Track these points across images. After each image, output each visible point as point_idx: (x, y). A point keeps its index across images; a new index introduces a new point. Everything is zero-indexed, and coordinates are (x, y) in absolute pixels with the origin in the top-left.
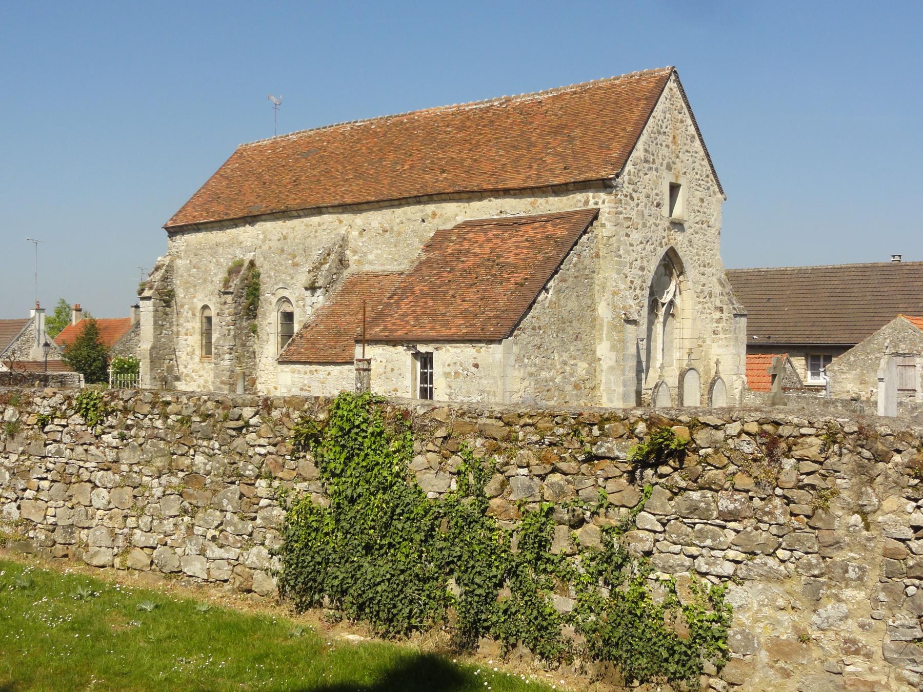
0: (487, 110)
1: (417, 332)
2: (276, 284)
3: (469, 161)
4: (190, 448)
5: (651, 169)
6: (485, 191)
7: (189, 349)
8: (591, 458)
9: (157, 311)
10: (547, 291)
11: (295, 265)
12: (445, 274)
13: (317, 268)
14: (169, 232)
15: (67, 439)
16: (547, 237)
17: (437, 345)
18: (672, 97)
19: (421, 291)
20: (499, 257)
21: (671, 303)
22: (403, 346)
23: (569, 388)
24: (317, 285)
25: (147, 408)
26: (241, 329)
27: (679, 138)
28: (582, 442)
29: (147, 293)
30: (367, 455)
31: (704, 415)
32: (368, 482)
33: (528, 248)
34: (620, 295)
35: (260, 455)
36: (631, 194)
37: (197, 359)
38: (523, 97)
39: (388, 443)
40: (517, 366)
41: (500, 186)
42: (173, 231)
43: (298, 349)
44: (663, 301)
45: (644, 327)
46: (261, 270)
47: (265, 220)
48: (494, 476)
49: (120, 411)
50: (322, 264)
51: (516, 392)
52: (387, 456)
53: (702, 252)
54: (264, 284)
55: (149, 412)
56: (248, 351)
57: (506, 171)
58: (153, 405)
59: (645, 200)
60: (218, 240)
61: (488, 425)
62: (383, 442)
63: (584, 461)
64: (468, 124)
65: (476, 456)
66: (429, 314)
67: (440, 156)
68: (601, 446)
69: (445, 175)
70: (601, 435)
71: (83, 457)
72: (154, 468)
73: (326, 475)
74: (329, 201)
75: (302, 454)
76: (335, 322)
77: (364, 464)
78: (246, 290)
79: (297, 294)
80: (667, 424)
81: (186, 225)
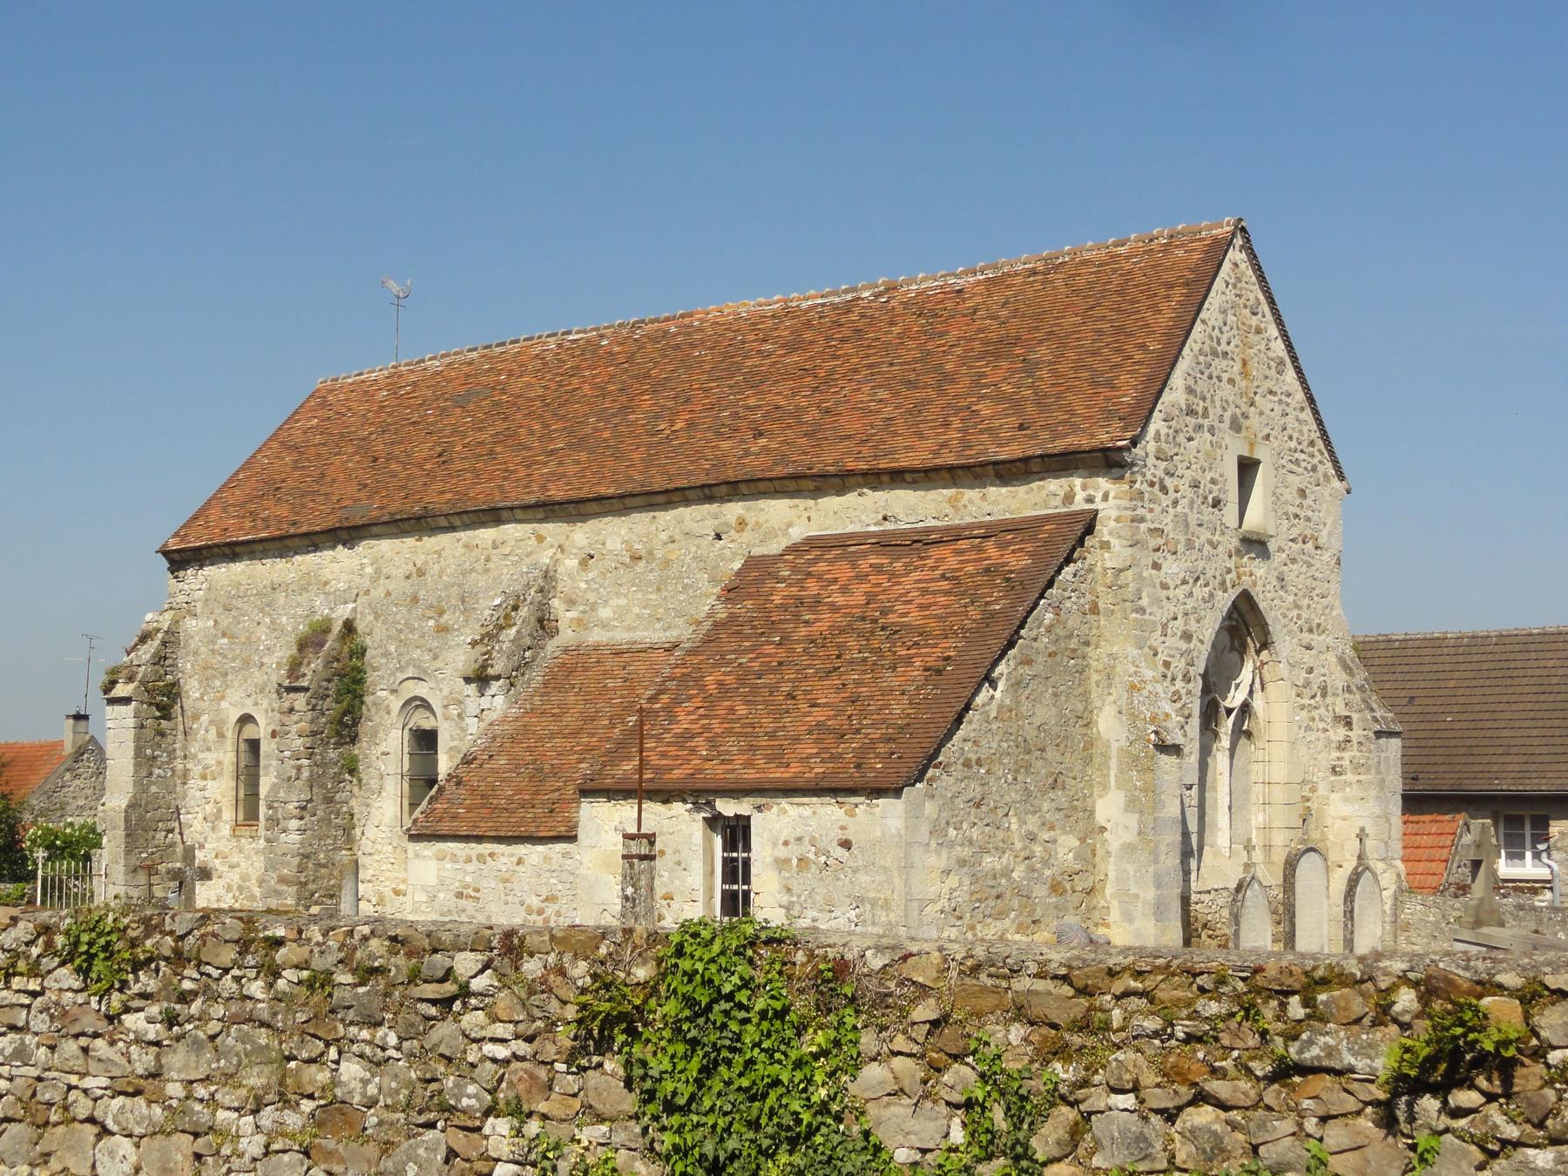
0: (848, 308)
1: (715, 771)
2: (401, 669)
3: (814, 412)
4: (328, 1045)
5: (1199, 427)
6: (852, 473)
7: (209, 808)
8: (1284, 1072)
9: (142, 727)
10: (993, 684)
11: (443, 630)
12: (770, 649)
13: (490, 636)
14: (171, 561)
15: (40, 1023)
16: (987, 570)
17: (760, 801)
18: (1239, 280)
19: (720, 684)
20: (884, 613)
21: (1246, 708)
22: (684, 801)
23: (1040, 891)
24: (490, 671)
25: (229, 954)
26: (324, 765)
27: (1253, 364)
28: (1264, 1034)
29: (121, 690)
30: (750, 1063)
31: (1556, 971)
32: (754, 1125)
33: (946, 593)
34: (1145, 692)
35: (494, 1060)
36: (1161, 481)
37: (226, 830)
38: (922, 281)
39: (799, 1035)
40: (933, 844)
41: (884, 464)
42: (180, 560)
43: (448, 807)
44: (1228, 703)
45: (1193, 759)
46: (368, 641)
47: (378, 537)
48: (1055, 1111)
49: (167, 959)
50: (501, 628)
51: (932, 901)
52: (799, 1064)
53: (1306, 602)
54: (375, 669)
55: (235, 962)
56: (338, 814)
57: (895, 434)
58: (244, 945)
59: (1189, 493)
60: (275, 577)
61: (1037, 993)
62: (789, 1033)
63: (1272, 1078)
64: (808, 336)
65: (1012, 1065)
66: (738, 734)
67: (751, 402)
68: (1311, 1042)
69: (763, 441)
70: (1308, 1017)
71: (78, 1064)
72: (244, 1092)
73: (651, 1109)
74: (517, 495)
75: (596, 1059)
76: (529, 749)
77: (745, 1083)
78: (336, 684)
79: (446, 692)
80: (1469, 993)
81: (208, 547)
